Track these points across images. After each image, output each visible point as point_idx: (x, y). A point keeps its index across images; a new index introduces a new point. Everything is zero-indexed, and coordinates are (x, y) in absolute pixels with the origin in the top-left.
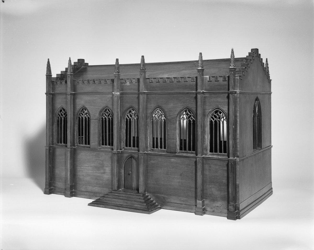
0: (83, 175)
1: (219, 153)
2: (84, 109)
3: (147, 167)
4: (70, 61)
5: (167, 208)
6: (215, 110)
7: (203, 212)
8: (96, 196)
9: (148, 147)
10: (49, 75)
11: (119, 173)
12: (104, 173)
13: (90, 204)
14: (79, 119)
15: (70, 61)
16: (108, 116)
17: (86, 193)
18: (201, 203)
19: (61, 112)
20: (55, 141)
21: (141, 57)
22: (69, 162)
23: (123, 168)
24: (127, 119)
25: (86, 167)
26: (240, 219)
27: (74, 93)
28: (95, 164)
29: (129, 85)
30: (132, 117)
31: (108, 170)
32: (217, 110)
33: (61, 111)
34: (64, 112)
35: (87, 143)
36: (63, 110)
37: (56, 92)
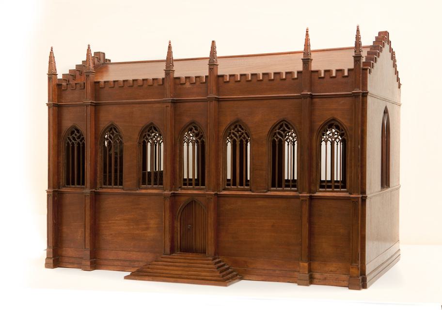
0: (111, 234)
1: (239, 187)
2: (112, 128)
3: (218, 215)
4: (89, 50)
5: (251, 279)
6: (339, 125)
7: (311, 281)
8: (134, 267)
9: (220, 184)
10: (52, 75)
11: (173, 228)
12: (147, 229)
13: (126, 278)
14: (143, 145)
15: (89, 50)
16: (240, 136)
17: (116, 263)
18: (307, 267)
19: (74, 135)
20: (63, 181)
21: (306, 30)
22: (88, 213)
23: (179, 220)
24: (68, 143)
25: (117, 220)
26: (364, 286)
27: (95, 103)
28: (132, 214)
29: (189, 86)
30: (75, 140)
31: (153, 223)
32: (333, 122)
33: (73, 132)
34: (78, 135)
35: (108, 182)
36: (76, 132)
37: (63, 101)
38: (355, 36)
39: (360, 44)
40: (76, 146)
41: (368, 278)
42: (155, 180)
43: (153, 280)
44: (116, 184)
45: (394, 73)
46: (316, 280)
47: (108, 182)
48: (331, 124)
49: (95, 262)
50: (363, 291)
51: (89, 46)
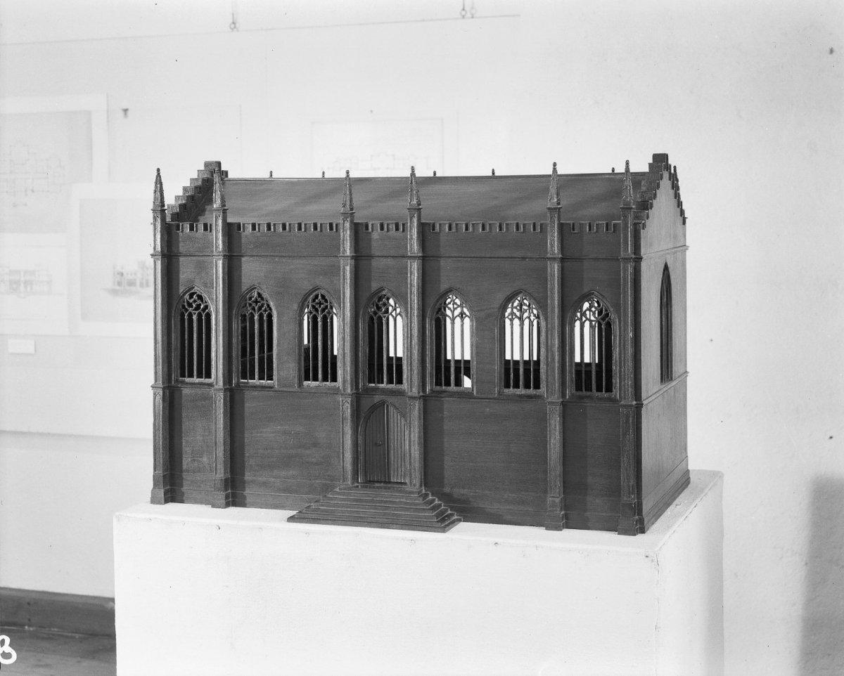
13: (291, 519)
26: (642, 530)
35: (376, 380)
38: (423, 172)
39: (388, 180)
40: (195, 317)
41: (645, 519)
42: (588, 373)
43: (409, 529)
44: (599, 389)
45: (676, 206)
46: (187, 482)
47: (376, 380)
48: (450, 291)
49: (234, 493)
50: (640, 537)
51: (158, 170)
